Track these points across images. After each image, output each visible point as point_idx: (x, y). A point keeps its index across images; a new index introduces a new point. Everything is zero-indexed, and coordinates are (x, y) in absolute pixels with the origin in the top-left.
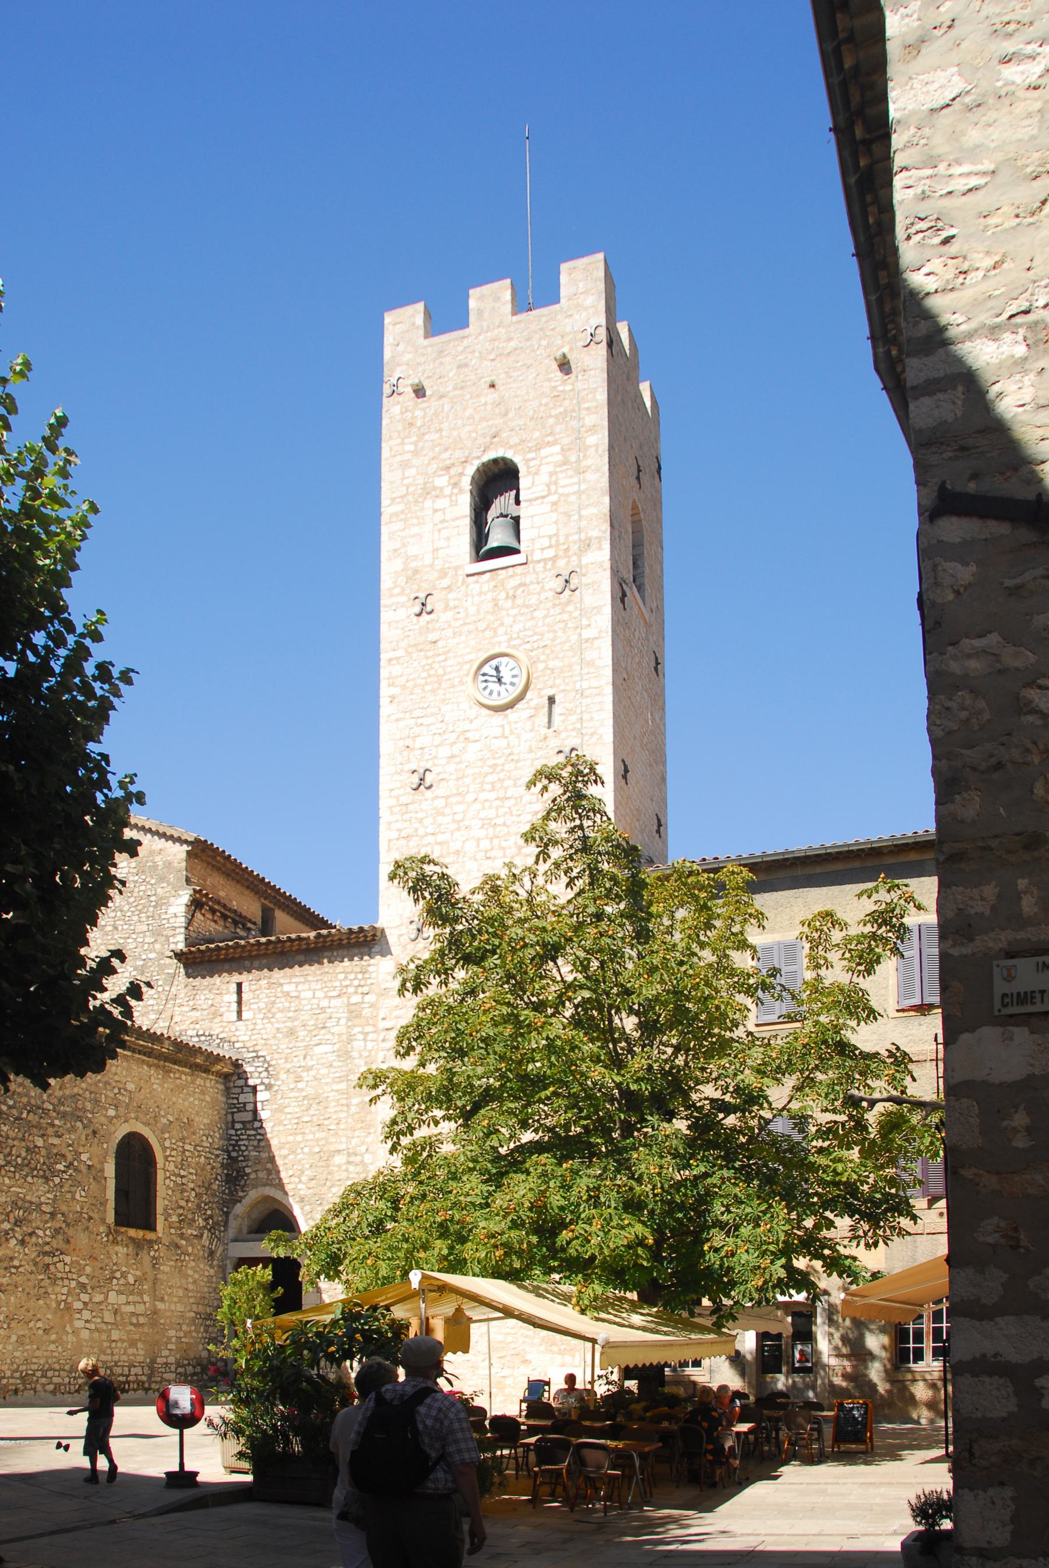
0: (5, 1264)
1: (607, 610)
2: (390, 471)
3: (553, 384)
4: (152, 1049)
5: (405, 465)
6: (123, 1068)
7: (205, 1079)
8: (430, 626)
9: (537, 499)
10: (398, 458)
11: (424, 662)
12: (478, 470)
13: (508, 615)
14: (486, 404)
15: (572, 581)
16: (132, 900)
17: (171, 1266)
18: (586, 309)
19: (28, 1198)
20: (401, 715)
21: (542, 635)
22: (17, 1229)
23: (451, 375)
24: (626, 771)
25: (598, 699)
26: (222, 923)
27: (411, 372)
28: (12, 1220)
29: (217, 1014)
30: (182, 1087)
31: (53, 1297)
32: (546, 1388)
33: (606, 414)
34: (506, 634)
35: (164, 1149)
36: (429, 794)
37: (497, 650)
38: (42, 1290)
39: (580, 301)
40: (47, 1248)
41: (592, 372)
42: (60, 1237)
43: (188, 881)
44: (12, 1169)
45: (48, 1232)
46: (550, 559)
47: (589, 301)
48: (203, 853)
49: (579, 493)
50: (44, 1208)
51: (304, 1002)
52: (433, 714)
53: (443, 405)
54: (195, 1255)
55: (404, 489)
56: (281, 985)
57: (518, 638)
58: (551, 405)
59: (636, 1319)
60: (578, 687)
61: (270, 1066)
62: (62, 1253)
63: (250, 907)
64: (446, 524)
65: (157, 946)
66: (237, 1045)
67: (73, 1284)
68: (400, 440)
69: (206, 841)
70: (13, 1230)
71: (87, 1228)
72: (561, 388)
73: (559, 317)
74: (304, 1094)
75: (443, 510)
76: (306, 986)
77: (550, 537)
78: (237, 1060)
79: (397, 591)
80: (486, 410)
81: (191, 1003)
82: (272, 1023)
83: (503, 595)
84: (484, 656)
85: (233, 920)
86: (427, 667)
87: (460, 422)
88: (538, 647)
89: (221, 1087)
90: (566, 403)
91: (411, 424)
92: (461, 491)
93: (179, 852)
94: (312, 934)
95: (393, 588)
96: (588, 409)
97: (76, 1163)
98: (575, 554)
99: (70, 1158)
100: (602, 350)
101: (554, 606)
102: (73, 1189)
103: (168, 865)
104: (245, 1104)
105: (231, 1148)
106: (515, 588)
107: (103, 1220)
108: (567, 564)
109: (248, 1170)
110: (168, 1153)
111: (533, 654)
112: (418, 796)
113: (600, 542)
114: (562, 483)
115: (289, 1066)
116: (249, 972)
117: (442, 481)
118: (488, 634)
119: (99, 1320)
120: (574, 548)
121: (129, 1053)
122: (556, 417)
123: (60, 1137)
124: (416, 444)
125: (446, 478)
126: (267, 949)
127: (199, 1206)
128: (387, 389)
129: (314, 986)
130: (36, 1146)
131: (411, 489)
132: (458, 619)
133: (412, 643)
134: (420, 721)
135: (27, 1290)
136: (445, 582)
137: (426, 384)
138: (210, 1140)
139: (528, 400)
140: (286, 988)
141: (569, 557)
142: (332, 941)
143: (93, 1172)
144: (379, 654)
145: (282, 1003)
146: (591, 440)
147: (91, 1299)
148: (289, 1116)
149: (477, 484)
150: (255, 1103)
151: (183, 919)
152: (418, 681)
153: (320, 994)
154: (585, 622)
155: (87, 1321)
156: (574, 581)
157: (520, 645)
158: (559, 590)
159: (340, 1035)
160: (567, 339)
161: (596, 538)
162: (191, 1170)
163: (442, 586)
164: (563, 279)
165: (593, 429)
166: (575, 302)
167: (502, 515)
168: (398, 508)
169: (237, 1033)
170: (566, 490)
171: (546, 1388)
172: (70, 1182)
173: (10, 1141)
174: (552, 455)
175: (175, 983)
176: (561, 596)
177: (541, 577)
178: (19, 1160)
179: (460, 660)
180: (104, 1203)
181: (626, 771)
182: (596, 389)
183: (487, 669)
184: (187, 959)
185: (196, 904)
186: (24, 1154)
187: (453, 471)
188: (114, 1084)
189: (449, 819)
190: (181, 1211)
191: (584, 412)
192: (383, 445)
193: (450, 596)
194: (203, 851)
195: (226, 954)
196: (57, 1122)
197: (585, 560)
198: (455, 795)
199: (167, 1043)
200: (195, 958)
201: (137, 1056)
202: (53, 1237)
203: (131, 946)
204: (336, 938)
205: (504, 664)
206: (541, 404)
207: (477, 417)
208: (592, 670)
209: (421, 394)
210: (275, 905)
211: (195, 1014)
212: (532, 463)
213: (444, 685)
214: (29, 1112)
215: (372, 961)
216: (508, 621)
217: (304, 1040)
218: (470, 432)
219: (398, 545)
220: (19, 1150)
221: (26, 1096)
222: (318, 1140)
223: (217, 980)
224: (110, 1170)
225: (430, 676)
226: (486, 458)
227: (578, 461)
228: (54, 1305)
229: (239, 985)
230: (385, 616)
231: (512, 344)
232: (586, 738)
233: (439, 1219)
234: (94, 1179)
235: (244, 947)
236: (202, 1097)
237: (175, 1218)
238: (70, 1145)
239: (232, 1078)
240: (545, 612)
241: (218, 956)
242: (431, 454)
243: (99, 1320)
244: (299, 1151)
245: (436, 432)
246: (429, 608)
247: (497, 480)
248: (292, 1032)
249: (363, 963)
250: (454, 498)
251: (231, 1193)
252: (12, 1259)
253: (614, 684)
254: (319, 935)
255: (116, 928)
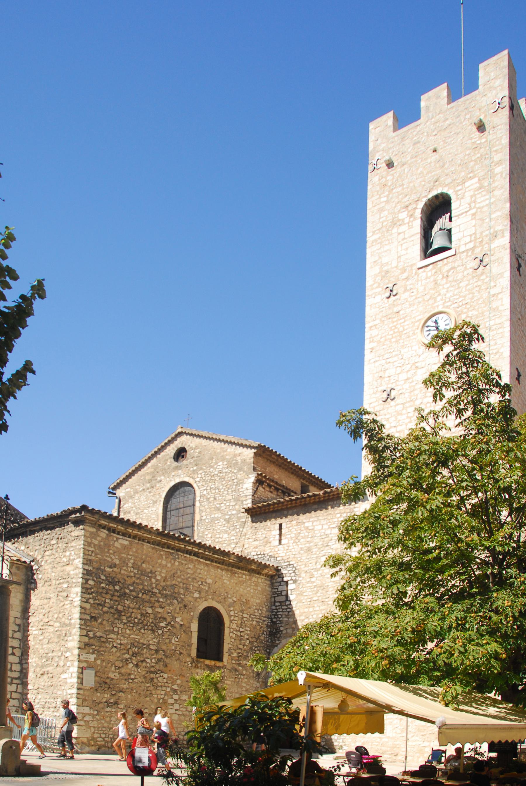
0: (126, 677)
1: (507, 274)
2: (372, 215)
3: (473, 141)
4: (224, 560)
5: (381, 210)
6: (205, 570)
7: (258, 578)
8: (395, 303)
9: (462, 214)
10: (376, 208)
11: (391, 325)
12: (426, 204)
13: (443, 288)
14: (431, 163)
15: (484, 261)
16: (224, 482)
17: (232, 681)
18: (495, 88)
19: (141, 641)
20: (377, 359)
21: (465, 297)
22: (134, 658)
23: (409, 150)
24: (519, 375)
25: (500, 331)
26: (275, 493)
27: (385, 154)
28: (131, 653)
29: (268, 542)
30: (242, 582)
31: (156, 696)
32: (444, 755)
33: (508, 151)
34: (442, 300)
35: (230, 616)
36: (393, 403)
37: (436, 310)
38: (148, 692)
39: (491, 84)
40: (152, 669)
41: (499, 127)
42: (161, 663)
43: (254, 469)
44: (132, 625)
45: (153, 661)
46: (471, 249)
47: (498, 83)
48: (263, 453)
49: (490, 205)
50: (151, 647)
51: (316, 532)
52: (396, 355)
53: (404, 170)
54: (248, 675)
55: (381, 224)
56: (304, 523)
57: (450, 301)
58: (472, 154)
59: (492, 710)
60: (487, 325)
61: (296, 569)
62: (162, 672)
63: (294, 484)
64: (405, 241)
65: (237, 507)
66: (278, 559)
67: (169, 689)
68: (378, 196)
69: (265, 446)
70: (131, 659)
71: (179, 659)
72: (478, 142)
73: (477, 98)
74: (315, 584)
75: (404, 232)
76: (318, 523)
77: (471, 236)
78: (277, 567)
79: (376, 285)
80: (430, 166)
81: (254, 537)
82: (298, 545)
83: (441, 276)
84: (428, 315)
85: (282, 491)
86: (393, 328)
87: (415, 177)
88: (462, 305)
89: (268, 582)
90: (482, 150)
91: (385, 185)
92: (415, 219)
93: (250, 453)
94: (321, 493)
95: (374, 284)
96: (496, 151)
97: (173, 623)
98: (487, 243)
99: (169, 620)
100: (506, 112)
101: (473, 277)
102: (170, 637)
103: (244, 461)
104: (281, 591)
105: (273, 617)
106: (448, 271)
107: (189, 655)
108: (481, 250)
109: (282, 629)
110: (232, 618)
111: (458, 310)
112: (386, 405)
113: (503, 233)
114: (478, 201)
115: (306, 569)
116: (286, 517)
117: (403, 215)
118: (431, 302)
119: (184, 710)
120: (486, 239)
121: (209, 562)
122: (475, 160)
123: (162, 608)
124: (387, 196)
125: (406, 212)
126: (296, 503)
127: (251, 649)
128: (370, 168)
129: (322, 522)
130: (147, 613)
131: (385, 224)
132: (412, 296)
133: (384, 315)
134: (388, 361)
135: (139, 692)
136: (405, 275)
137: (394, 159)
138: (260, 612)
139: (457, 154)
140: (307, 525)
141: (483, 246)
142: (333, 495)
143: (184, 628)
144: (365, 324)
145: (304, 533)
146: (498, 170)
147: (179, 698)
148: (306, 597)
149: (426, 214)
150: (287, 591)
151: (251, 491)
152: (388, 337)
153: (325, 527)
154: (492, 284)
155: (177, 710)
156: (486, 260)
157: (451, 305)
158: (476, 267)
159: (336, 549)
160: (483, 110)
161: (501, 230)
162: (247, 629)
163: (403, 278)
164: (481, 74)
165: (499, 163)
166: (488, 86)
167: (441, 229)
168: (376, 236)
169: (279, 552)
170: (481, 205)
171: (444, 755)
172: (168, 633)
173: (131, 610)
174: (472, 185)
175: (246, 526)
176: (478, 271)
177: (465, 261)
178: (136, 620)
179: (414, 320)
180: (190, 645)
181: (519, 375)
182: (501, 137)
183: (430, 323)
184: (252, 512)
185: (259, 482)
186: (139, 617)
187: (410, 208)
188: (198, 579)
189: (404, 417)
190: (240, 651)
191: (494, 154)
192: (368, 201)
193: (408, 283)
194: (264, 452)
195: (274, 508)
196: (161, 600)
197: (492, 246)
198: (409, 402)
199: (232, 557)
200: (256, 511)
201: (214, 564)
202: (156, 663)
203: (223, 508)
204: (335, 493)
205: (440, 318)
206: (466, 155)
207: (425, 172)
208: (496, 313)
209: (390, 166)
210: (309, 483)
211: (256, 543)
212: (459, 193)
213: (403, 337)
214: (143, 594)
215: (356, 505)
216: (443, 292)
217: (315, 554)
218: (421, 182)
219: (377, 258)
220: (137, 615)
221: (142, 584)
222: (321, 610)
223: (268, 523)
224: (195, 627)
225: (394, 333)
226: (430, 196)
227: (490, 184)
228: (156, 700)
229: (281, 525)
230: (369, 301)
231: (448, 122)
232: (492, 356)
233: (349, 642)
234: (184, 632)
235: (283, 503)
236: (255, 588)
237: (235, 655)
238: (169, 613)
239: (275, 577)
240: (467, 282)
241: (269, 509)
242: (397, 200)
243: (184, 710)
244: (311, 617)
245: (400, 186)
246: (394, 293)
247: (439, 207)
248: (309, 550)
249: (351, 507)
250: (410, 224)
251: (272, 641)
252: (130, 674)
253: (511, 320)
254: (326, 493)
255: (215, 499)
